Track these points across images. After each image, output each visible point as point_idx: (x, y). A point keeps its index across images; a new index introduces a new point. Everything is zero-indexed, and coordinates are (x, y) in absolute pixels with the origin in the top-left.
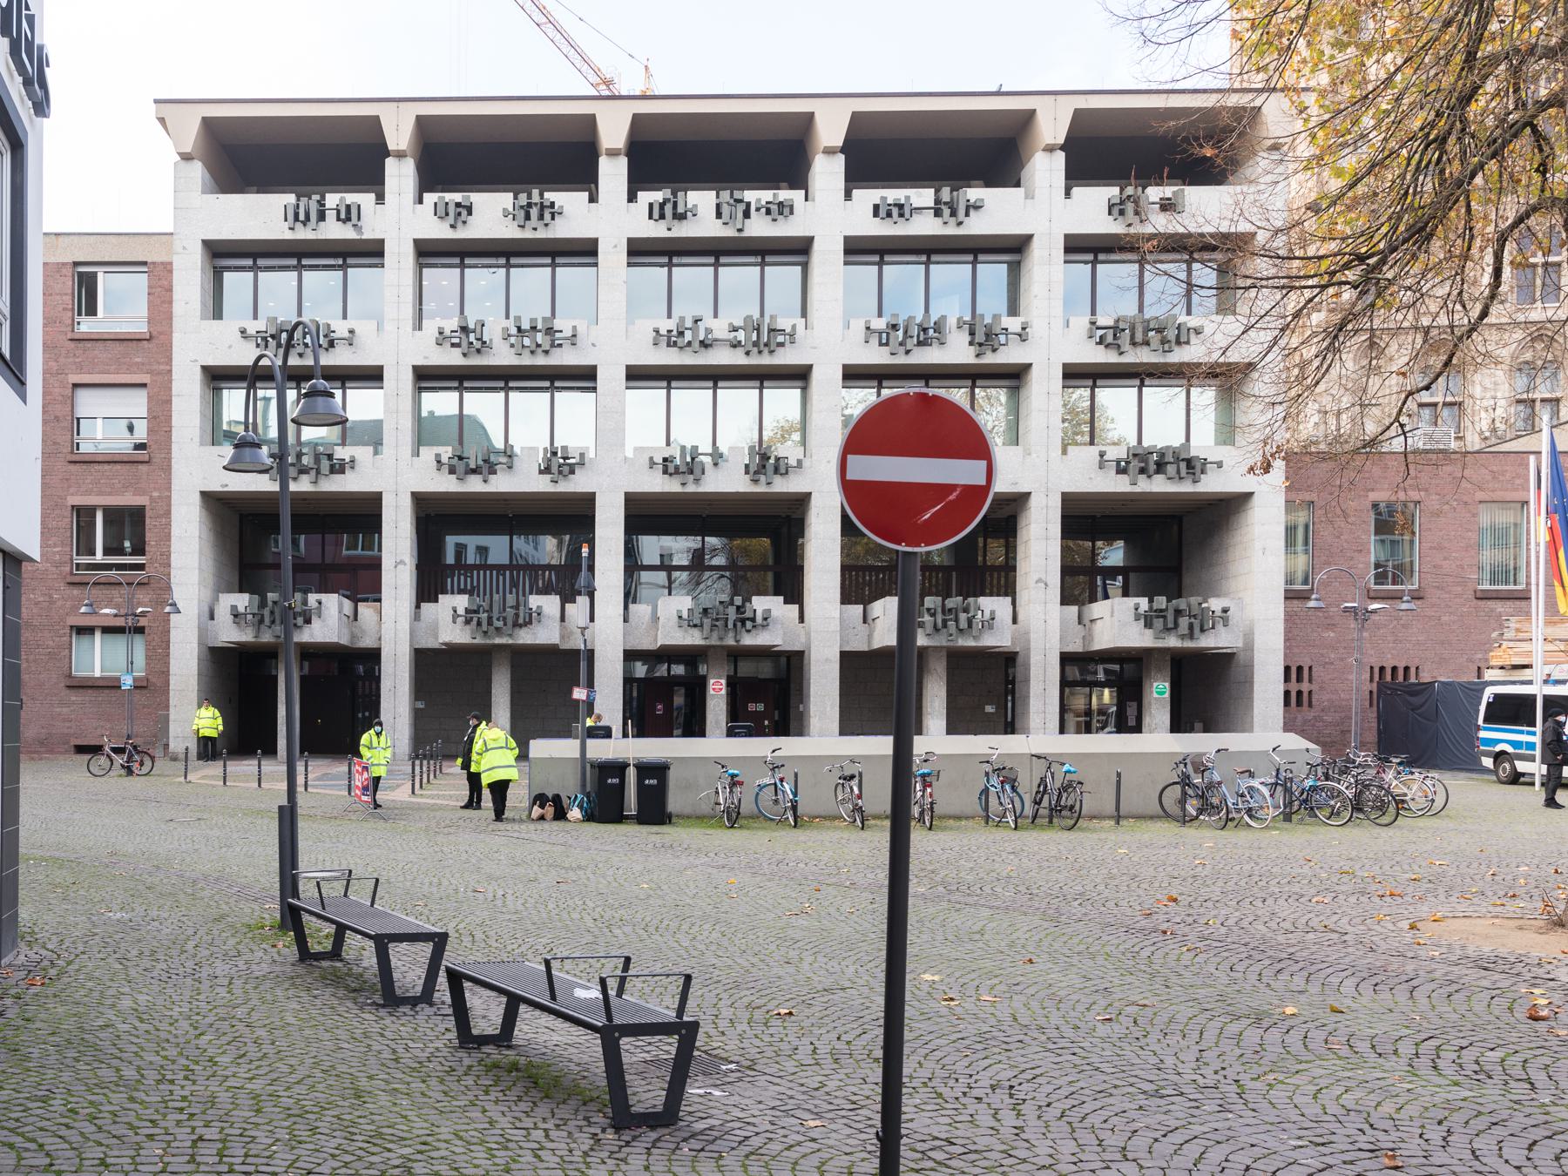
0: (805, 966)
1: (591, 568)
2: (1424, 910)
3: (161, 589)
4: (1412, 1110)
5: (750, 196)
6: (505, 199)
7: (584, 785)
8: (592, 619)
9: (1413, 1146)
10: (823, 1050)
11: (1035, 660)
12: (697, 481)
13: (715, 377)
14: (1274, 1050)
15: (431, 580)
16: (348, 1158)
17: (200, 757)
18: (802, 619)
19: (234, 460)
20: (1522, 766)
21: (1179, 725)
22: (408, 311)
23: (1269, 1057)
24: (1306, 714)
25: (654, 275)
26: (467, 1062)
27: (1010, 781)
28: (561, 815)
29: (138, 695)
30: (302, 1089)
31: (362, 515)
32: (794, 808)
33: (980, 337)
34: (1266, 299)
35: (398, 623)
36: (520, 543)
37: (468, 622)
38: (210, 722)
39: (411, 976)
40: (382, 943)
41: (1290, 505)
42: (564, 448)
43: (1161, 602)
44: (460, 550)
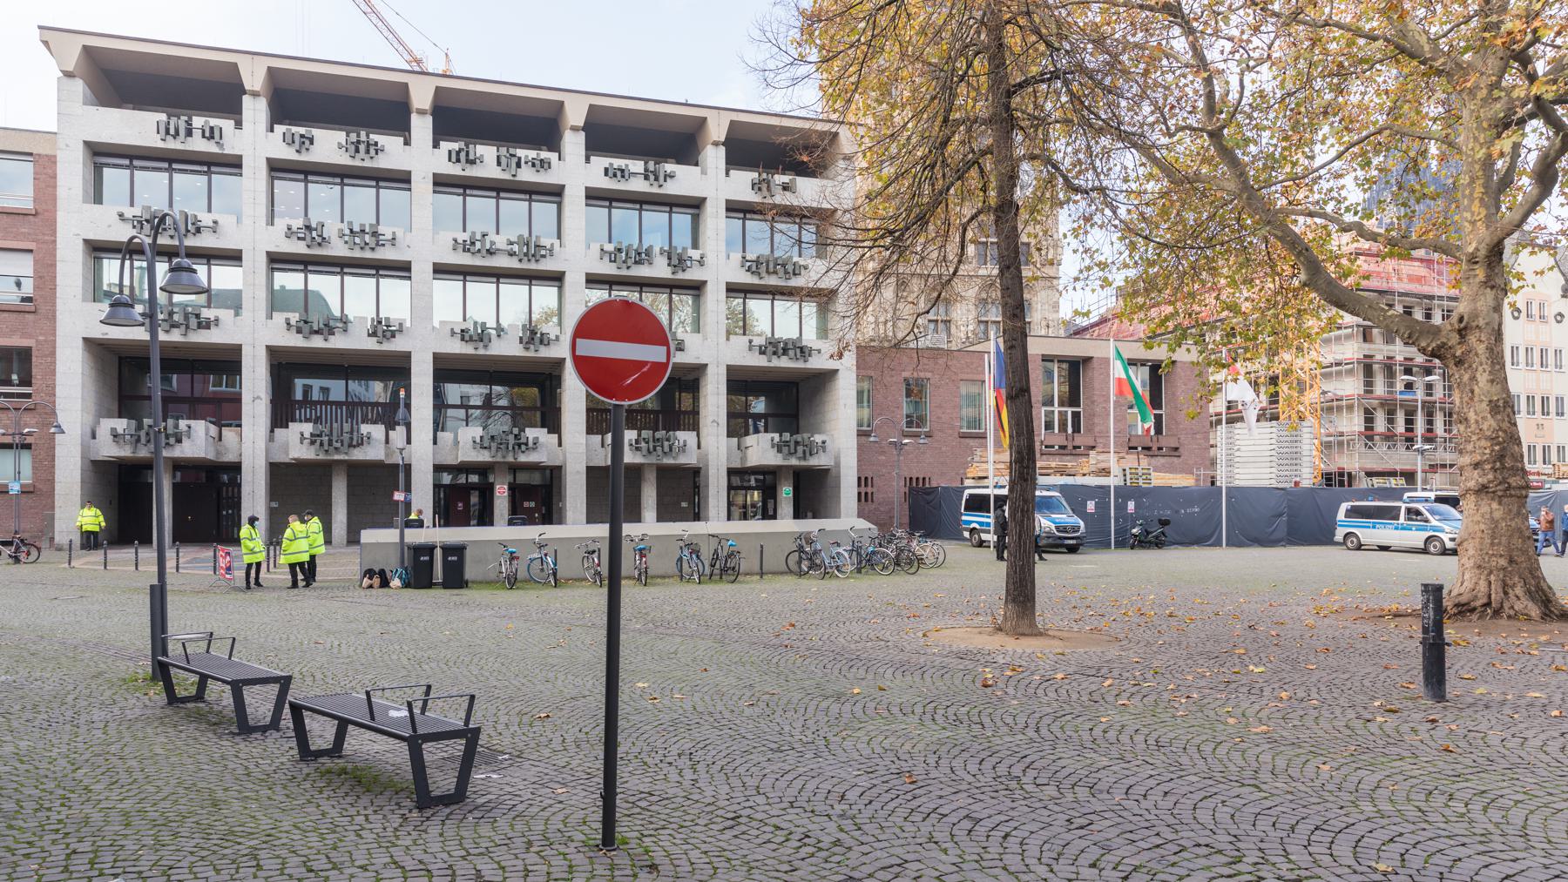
0: (559, 683)
1: (408, 406)
2: (931, 625)
3: (48, 413)
4: (920, 746)
5: (521, 153)
6: (340, 136)
7: (402, 562)
8: (409, 442)
9: (919, 770)
10: (569, 739)
11: (712, 472)
12: (486, 347)
13: (498, 275)
14: (847, 716)
15: (282, 412)
16: (204, 853)
17: (83, 547)
18: (560, 445)
19: (110, 316)
20: (984, 537)
21: (798, 514)
22: (262, 210)
23: (844, 720)
24: (870, 506)
25: (453, 201)
26: (306, 770)
27: (696, 552)
28: (385, 583)
29: (24, 498)
30: (167, 804)
31: (227, 362)
32: (555, 574)
33: (675, 261)
34: (840, 252)
35: (255, 443)
36: (354, 386)
37: (313, 443)
38: (92, 520)
39: (262, 710)
40: (237, 687)
41: (860, 379)
42: (387, 319)
43: (787, 436)
44: (307, 390)
